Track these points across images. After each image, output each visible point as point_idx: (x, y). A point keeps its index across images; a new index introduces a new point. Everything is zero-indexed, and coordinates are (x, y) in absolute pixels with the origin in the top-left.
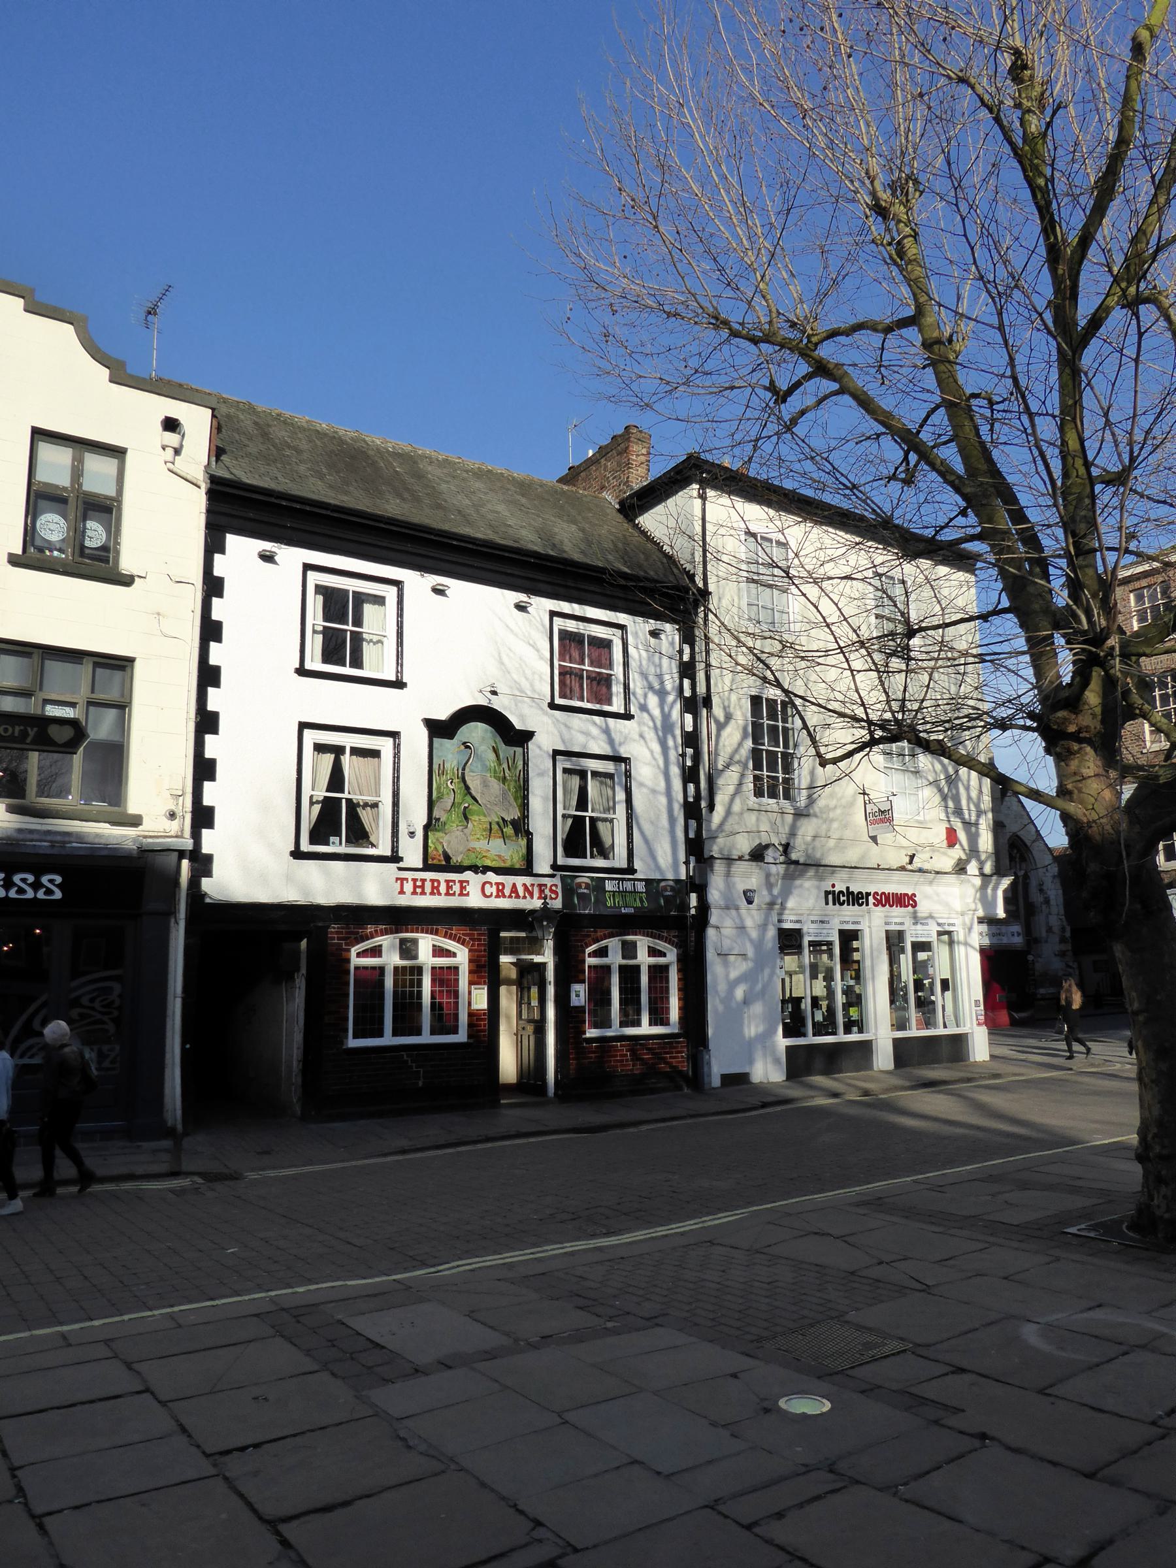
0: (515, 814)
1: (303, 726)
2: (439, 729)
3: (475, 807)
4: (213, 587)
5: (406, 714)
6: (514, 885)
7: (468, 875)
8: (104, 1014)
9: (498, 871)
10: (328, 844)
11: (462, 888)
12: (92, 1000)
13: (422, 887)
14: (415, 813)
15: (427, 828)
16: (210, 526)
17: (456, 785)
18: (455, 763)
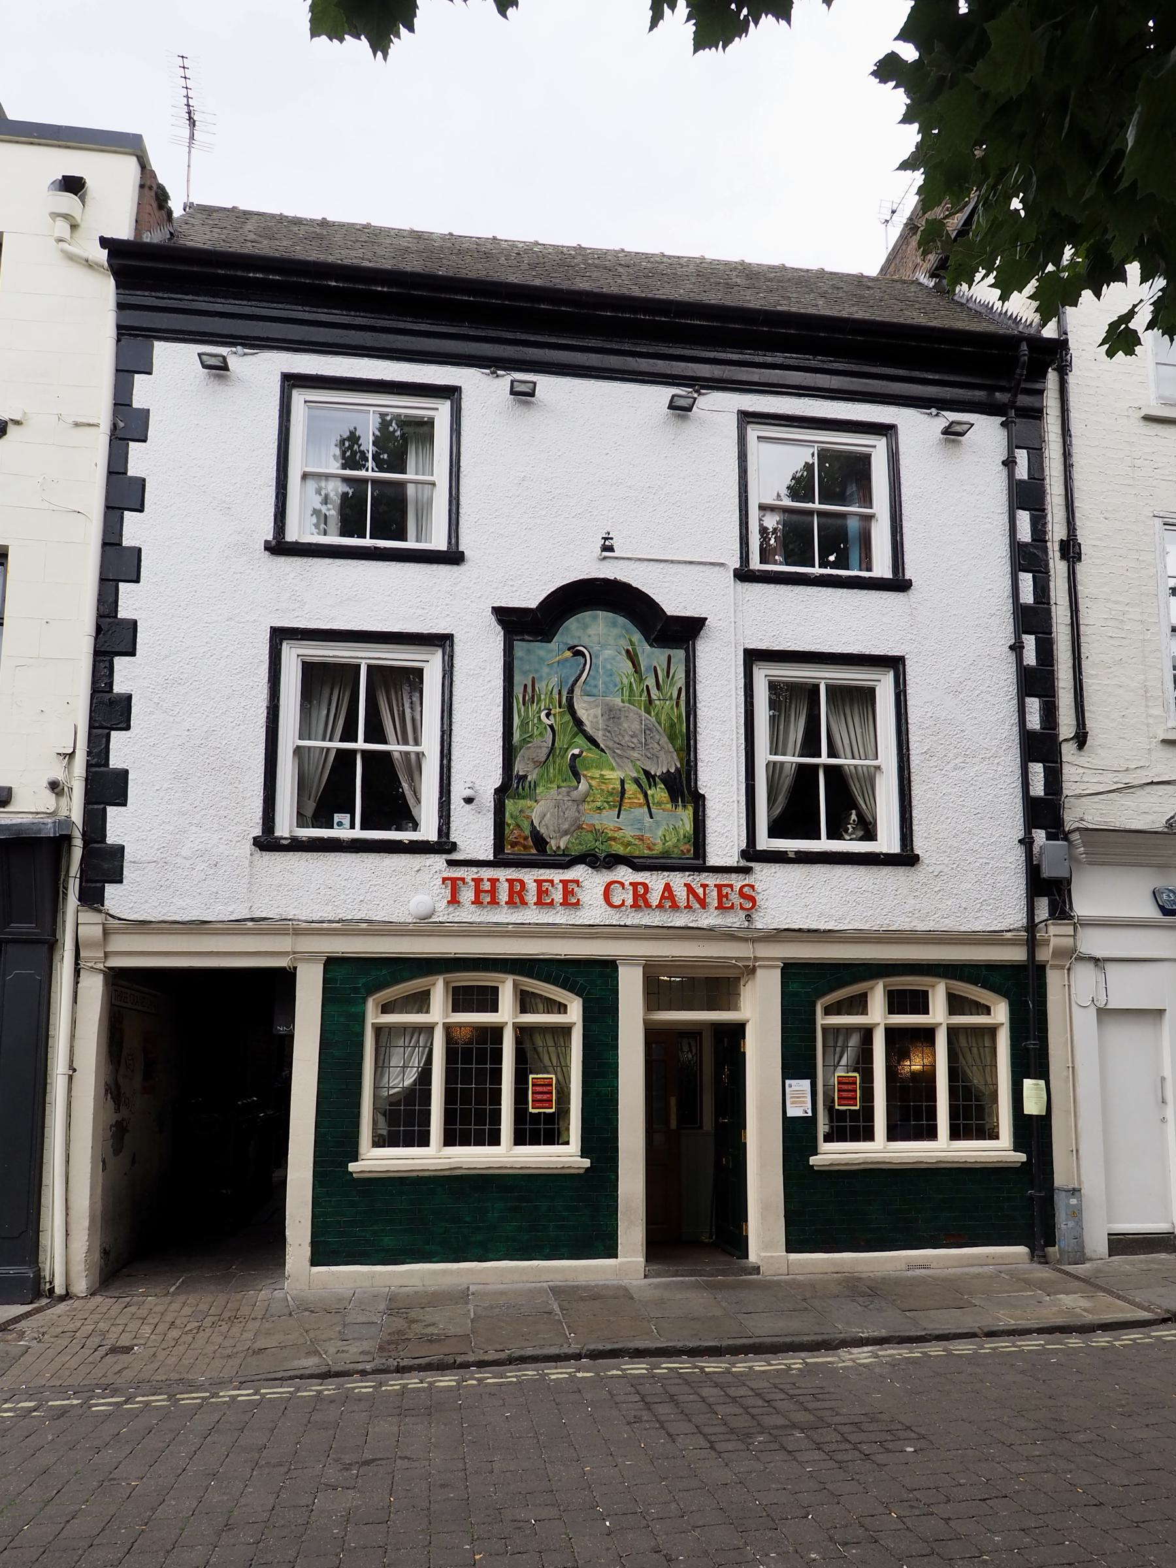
0: (667, 763)
1: (280, 636)
2: (515, 624)
3: (591, 754)
4: (128, 425)
5: (459, 605)
6: (667, 887)
7: (578, 872)
9: (636, 865)
11: (567, 893)
13: (493, 892)
14: (479, 766)
15: (501, 793)
16: (123, 331)
17: (559, 719)
18: (555, 680)
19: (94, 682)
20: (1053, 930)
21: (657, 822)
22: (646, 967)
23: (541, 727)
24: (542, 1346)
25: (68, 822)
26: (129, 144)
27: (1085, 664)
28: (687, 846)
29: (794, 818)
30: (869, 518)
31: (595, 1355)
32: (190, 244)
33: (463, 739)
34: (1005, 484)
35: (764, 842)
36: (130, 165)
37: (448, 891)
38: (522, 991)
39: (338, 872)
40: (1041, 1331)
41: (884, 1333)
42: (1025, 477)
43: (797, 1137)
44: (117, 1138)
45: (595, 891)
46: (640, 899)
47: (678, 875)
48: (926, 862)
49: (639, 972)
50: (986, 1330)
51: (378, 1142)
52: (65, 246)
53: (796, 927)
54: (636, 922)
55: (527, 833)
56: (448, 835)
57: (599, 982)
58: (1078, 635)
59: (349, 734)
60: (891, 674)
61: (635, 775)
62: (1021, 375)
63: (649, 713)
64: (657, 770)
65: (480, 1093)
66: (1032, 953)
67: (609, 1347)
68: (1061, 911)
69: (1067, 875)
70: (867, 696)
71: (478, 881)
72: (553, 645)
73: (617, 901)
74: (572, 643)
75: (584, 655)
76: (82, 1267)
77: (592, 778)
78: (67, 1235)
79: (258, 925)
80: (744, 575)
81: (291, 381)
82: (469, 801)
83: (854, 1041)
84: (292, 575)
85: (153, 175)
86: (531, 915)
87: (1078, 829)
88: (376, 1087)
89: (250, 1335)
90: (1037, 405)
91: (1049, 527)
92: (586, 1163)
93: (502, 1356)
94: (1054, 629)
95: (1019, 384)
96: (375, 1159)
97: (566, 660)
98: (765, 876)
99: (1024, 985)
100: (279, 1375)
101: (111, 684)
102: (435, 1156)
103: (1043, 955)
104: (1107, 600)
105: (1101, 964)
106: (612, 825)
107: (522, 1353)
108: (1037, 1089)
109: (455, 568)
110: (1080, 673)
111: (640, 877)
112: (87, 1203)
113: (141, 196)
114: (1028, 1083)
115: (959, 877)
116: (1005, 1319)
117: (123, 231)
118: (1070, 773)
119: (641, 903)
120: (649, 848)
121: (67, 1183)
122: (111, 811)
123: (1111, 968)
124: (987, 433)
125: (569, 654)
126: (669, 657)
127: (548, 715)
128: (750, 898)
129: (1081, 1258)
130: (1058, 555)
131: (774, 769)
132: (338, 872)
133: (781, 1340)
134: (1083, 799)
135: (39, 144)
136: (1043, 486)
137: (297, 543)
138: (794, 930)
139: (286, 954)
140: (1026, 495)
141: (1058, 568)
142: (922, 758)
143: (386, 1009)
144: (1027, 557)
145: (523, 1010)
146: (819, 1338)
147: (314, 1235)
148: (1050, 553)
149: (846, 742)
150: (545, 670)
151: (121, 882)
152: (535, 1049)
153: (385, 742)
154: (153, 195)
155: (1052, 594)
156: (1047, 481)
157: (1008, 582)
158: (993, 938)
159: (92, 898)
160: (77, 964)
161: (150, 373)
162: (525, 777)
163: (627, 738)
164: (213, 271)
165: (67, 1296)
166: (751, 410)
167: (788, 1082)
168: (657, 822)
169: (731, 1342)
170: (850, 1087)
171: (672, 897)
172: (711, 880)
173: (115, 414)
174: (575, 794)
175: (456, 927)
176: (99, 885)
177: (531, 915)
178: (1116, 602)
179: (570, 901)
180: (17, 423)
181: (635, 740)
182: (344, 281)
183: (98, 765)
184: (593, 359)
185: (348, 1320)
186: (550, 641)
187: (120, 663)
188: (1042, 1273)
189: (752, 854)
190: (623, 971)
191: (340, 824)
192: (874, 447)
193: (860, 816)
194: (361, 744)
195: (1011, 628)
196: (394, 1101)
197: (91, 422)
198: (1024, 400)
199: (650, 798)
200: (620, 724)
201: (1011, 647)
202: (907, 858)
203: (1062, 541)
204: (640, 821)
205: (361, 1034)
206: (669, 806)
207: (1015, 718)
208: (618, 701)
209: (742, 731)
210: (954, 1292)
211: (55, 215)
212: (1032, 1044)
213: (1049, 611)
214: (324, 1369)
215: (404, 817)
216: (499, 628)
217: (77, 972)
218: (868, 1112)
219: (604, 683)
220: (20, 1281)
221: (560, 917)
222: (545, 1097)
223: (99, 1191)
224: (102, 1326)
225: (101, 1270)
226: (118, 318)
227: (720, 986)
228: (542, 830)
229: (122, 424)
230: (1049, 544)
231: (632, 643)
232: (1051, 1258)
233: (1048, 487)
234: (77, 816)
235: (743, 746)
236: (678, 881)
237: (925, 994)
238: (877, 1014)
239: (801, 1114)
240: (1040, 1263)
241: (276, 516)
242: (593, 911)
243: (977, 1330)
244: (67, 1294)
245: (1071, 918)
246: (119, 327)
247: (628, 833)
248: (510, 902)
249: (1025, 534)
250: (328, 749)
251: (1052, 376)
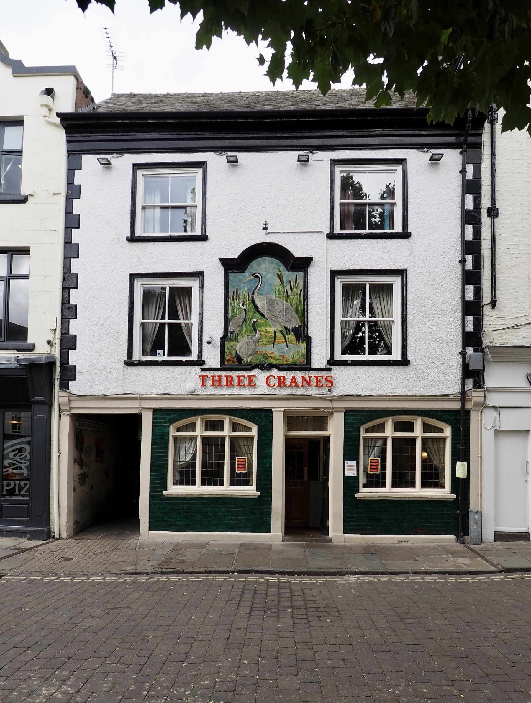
0: (295, 323)
1: (133, 277)
2: (230, 265)
3: (261, 321)
4: (73, 192)
5: (206, 259)
6: (294, 378)
7: (256, 372)
8: (21, 463)
9: (281, 368)
11: (250, 381)
12: (15, 455)
13: (220, 381)
14: (214, 329)
15: (223, 339)
16: (70, 152)
17: (248, 306)
19: (62, 300)
20: (474, 394)
21: (290, 349)
22: (284, 412)
23: (240, 310)
24: (220, 567)
25: (54, 357)
26: (70, 71)
27: (497, 267)
28: (303, 360)
29: (353, 346)
30: (393, 204)
31: (240, 572)
32: (102, 111)
33: (207, 318)
34: (460, 183)
35: (338, 356)
36: (71, 81)
37: (201, 381)
38: (233, 422)
39: (157, 374)
40: (439, 573)
41: (367, 570)
42: (471, 178)
43: (351, 485)
44: (81, 479)
45: (263, 380)
46: (282, 383)
47: (299, 372)
48: (414, 364)
49: (281, 414)
50: (413, 571)
52: (47, 118)
53: (351, 394)
54: (280, 393)
55: (234, 356)
56: (201, 357)
57: (264, 419)
58: (494, 254)
59: (163, 318)
60: (400, 277)
61: (280, 329)
62: (469, 127)
63: (287, 302)
64: (290, 327)
66: (463, 405)
67: (246, 569)
68: (479, 385)
69: (481, 368)
70: (388, 289)
71: (213, 377)
72: (246, 274)
74: (253, 272)
75: (258, 277)
76: (65, 528)
77: (262, 331)
78: (59, 515)
79: (126, 396)
80: (331, 236)
81: (137, 167)
82: (209, 343)
83: (379, 444)
84: (138, 251)
85: (82, 83)
86: (236, 391)
87: (487, 346)
88: (175, 462)
89: (116, 556)
90: (479, 141)
91: (482, 201)
93: (202, 570)
94: (482, 252)
95: (468, 132)
96: (174, 490)
97: (251, 280)
98: (338, 372)
99: (460, 420)
100: (116, 572)
101: (69, 301)
102: (198, 489)
103: (469, 405)
104: (511, 235)
105: (498, 409)
106: (270, 351)
107: (211, 569)
108: (463, 466)
109: (204, 243)
110: (495, 272)
111: (282, 373)
112: (66, 504)
113: (77, 93)
114: (459, 463)
115: (431, 369)
116: (427, 567)
117: (69, 108)
118: (487, 320)
119: (282, 385)
120: (286, 361)
121: (59, 496)
122: (71, 351)
123: (503, 412)
124: (452, 158)
125: (252, 277)
126: (297, 276)
127: (243, 305)
128: (330, 382)
129: (481, 541)
130: (486, 215)
131: (345, 325)
132: (157, 374)
133: (320, 570)
134: (494, 332)
135: (36, 76)
136: (480, 181)
137: (139, 237)
138: (350, 396)
139: (137, 408)
140: (471, 187)
141: (486, 221)
142: (414, 316)
143: (178, 430)
144: (471, 217)
145: (234, 430)
146: (337, 570)
147: (150, 519)
148: (482, 214)
149: (380, 310)
150: (242, 285)
151: (75, 380)
152: (240, 446)
153: (179, 320)
154: (84, 93)
155: (482, 234)
156: (482, 179)
157: (460, 230)
158: (445, 398)
159: (64, 386)
160: (60, 412)
161: (81, 169)
162: (233, 332)
163: (277, 313)
164: (101, 122)
165: (60, 538)
166: (336, 158)
167: (346, 461)
168: (290, 349)
169: (297, 570)
170: (375, 464)
171: (295, 382)
172: (313, 374)
173: (68, 188)
175: (204, 396)
176: (67, 381)
177: (236, 391)
178: (516, 236)
179: (252, 384)
180: (32, 196)
181: (281, 314)
182: (174, 119)
183: (65, 334)
184: (264, 142)
185: (155, 553)
186: (244, 272)
187: (72, 291)
188: (459, 547)
189: (332, 362)
190: (275, 414)
191: (159, 354)
192: (396, 170)
193: (385, 344)
194: (167, 321)
195: (460, 252)
196: (182, 467)
197: (59, 192)
198: (471, 140)
199: (287, 339)
200: (274, 307)
201: (460, 262)
202: (404, 362)
203: (488, 208)
204: (283, 349)
205: (168, 440)
206: (295, 342)
207: (460, 295)
208: (273, 297)
209: (329, 307)
210: (411, 553)
211: (42, 106)
212: (461, 446)
213: (480, 243)
214: (133, 571)
215: (187, 351)
216: (223, 268)
217: (60, 415)
218: (384, 475)
219: (268, 289)
220: (42, 532)
221: (248, 391)
222: (242, 466)
223: (72, 499)
224: (66, 550)
225: (74, 529)
226: (67, 148)
227: (320, 421)
228: (240, 355)
229: (70, 192)
230: (482, 210)
231: (280, 271)
232: (466, 541)
233: (482, 182)
234: (57, 354)
235: (329, 314)
236: (298, 375)
237: (412, 423)
238: (389, 432)
239: (352, 475)
240: (460, 543)
241: (131, 226)
242: (262, 388)
243: (410, 571)
244: (60, 537)
245: (483, 388)
246: (68, 151)
247: (277, 355)
248: (227, 385)
249: (469, 206)
250: (156, 324)
251: (487, 126)
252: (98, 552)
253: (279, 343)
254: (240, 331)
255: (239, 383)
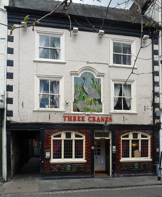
3: (86, 96)
10: (45, 107)
13: (71, 118)
18: (80, 84)
24: (96, 186)
51: (54, 158)
61: (93, 99)
65: (78, 151)
73: (90, 120)
92: (86, 161)
130: (160, 63)
143: (54, 137)
174: (84, 102)
206: (99, 104)
228: (79, 108)
246: (8, 21)
252: (101, 151)
253: (93, 104)
254: (78, 99)
255: (82, 119)
